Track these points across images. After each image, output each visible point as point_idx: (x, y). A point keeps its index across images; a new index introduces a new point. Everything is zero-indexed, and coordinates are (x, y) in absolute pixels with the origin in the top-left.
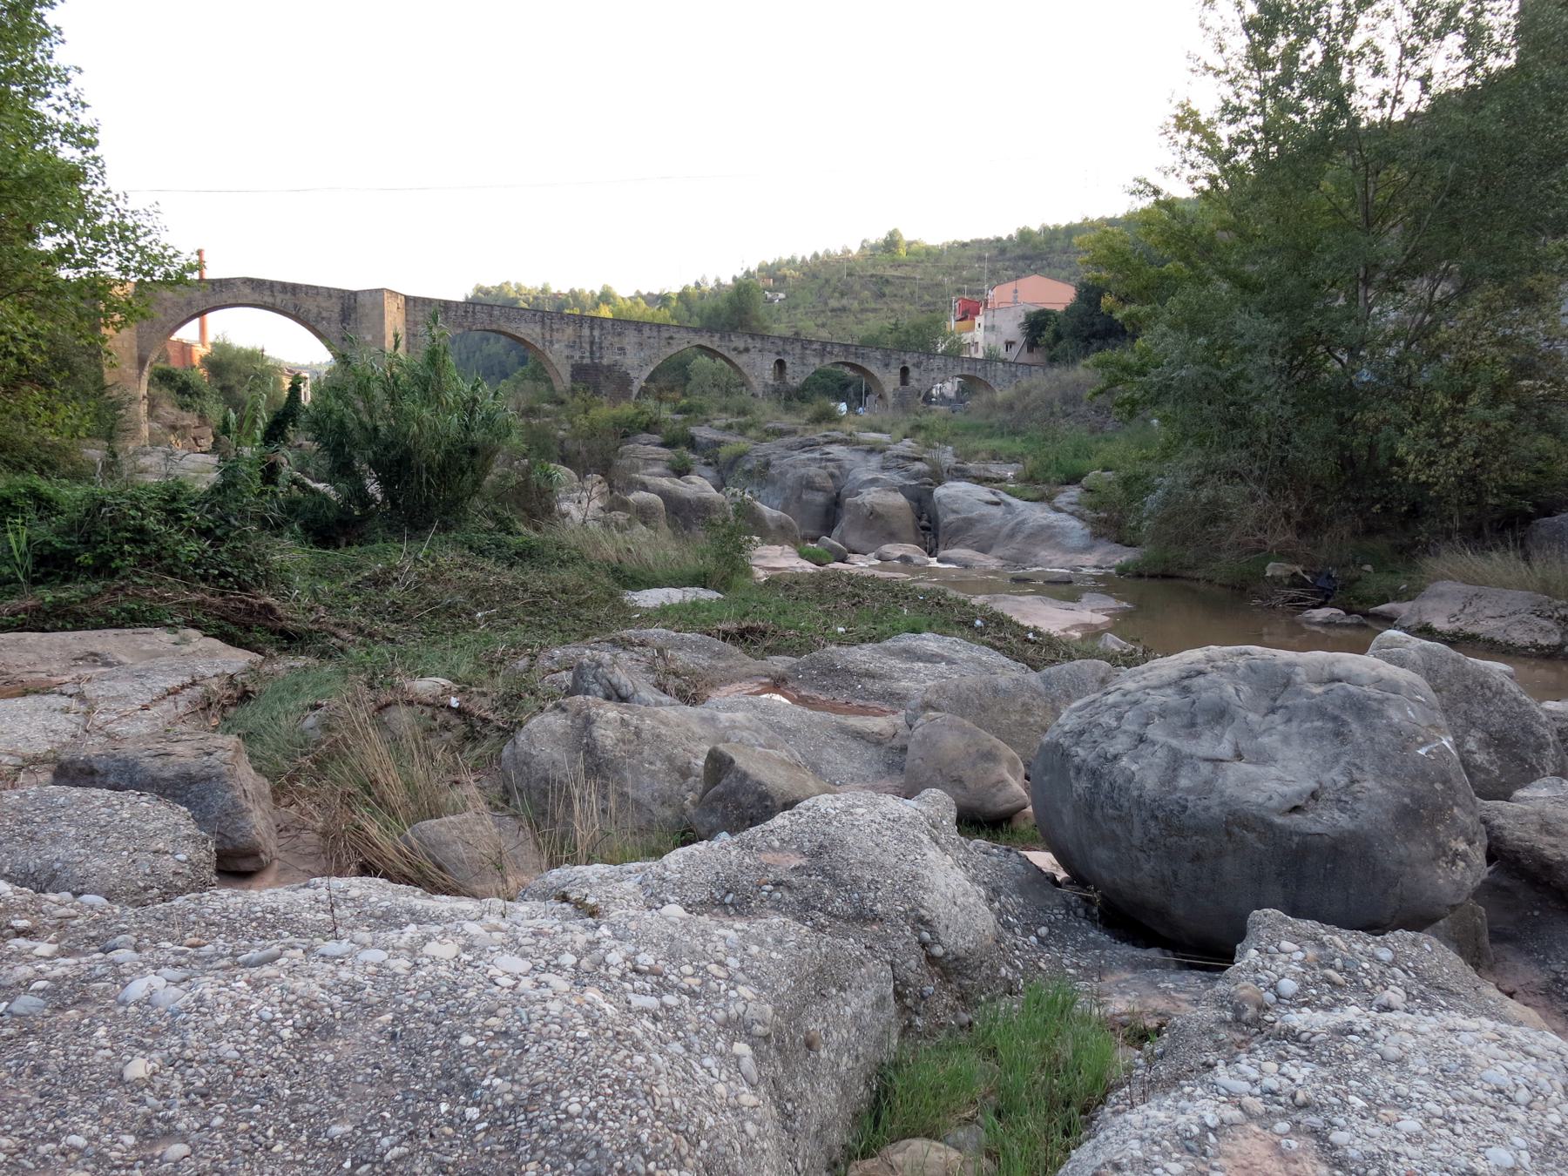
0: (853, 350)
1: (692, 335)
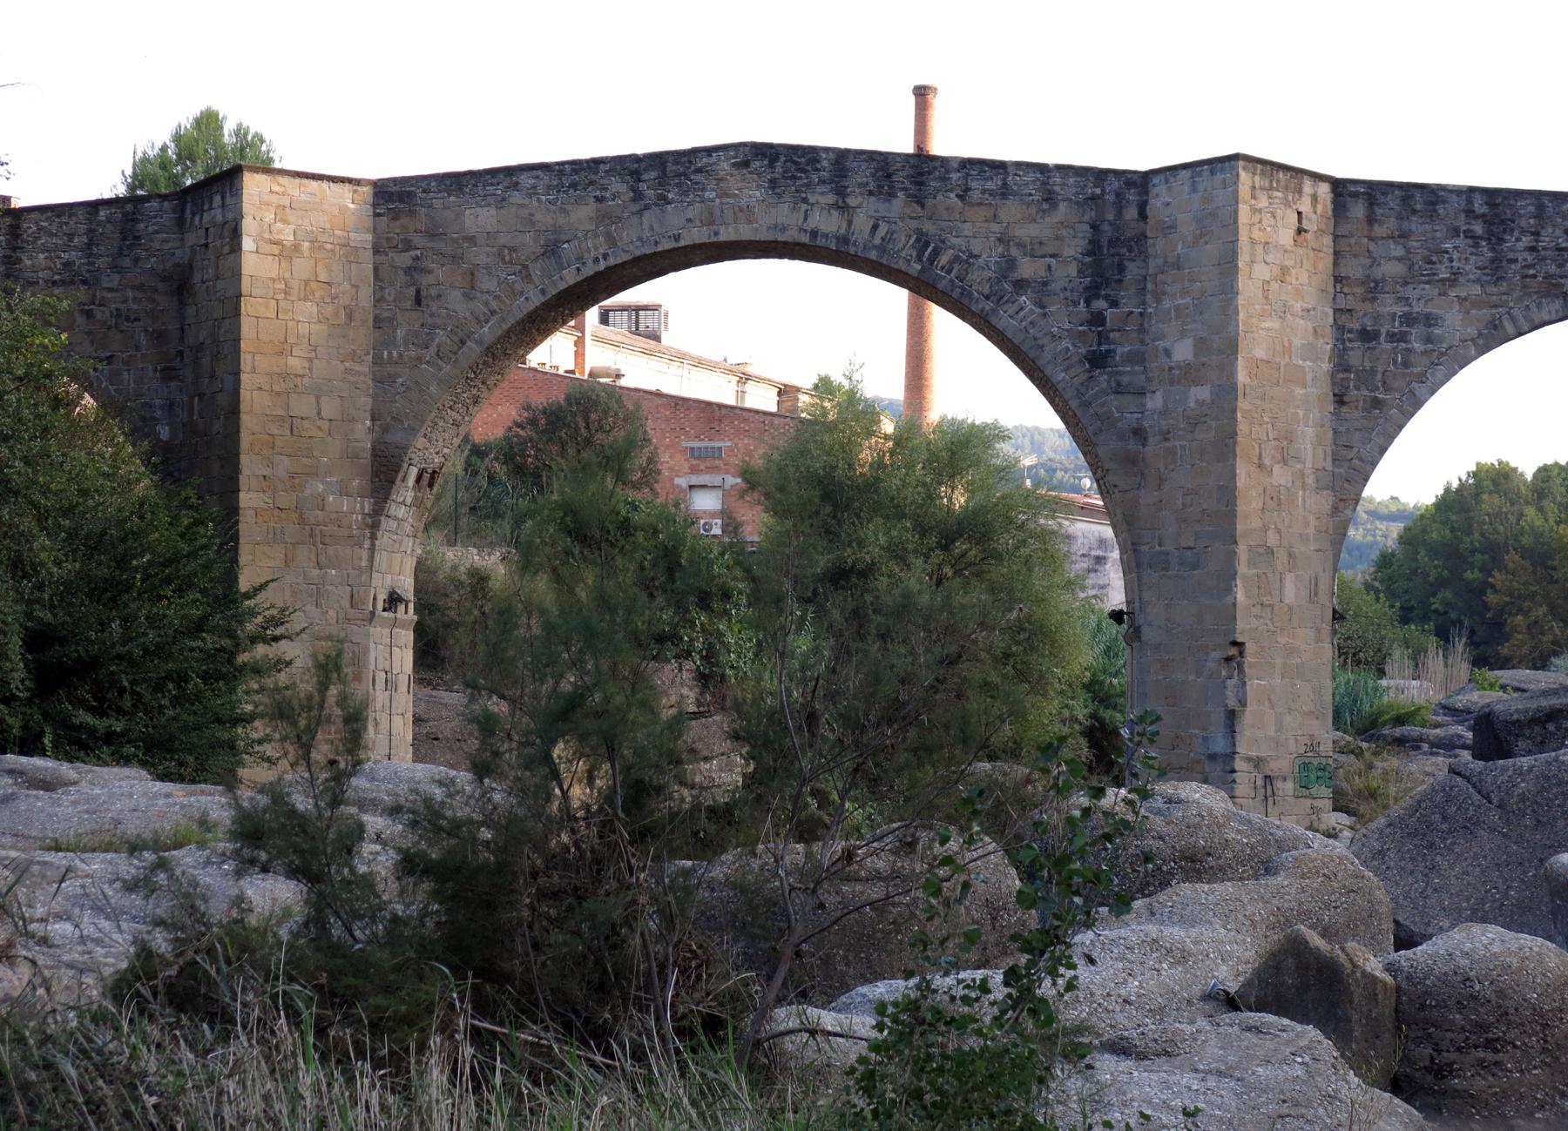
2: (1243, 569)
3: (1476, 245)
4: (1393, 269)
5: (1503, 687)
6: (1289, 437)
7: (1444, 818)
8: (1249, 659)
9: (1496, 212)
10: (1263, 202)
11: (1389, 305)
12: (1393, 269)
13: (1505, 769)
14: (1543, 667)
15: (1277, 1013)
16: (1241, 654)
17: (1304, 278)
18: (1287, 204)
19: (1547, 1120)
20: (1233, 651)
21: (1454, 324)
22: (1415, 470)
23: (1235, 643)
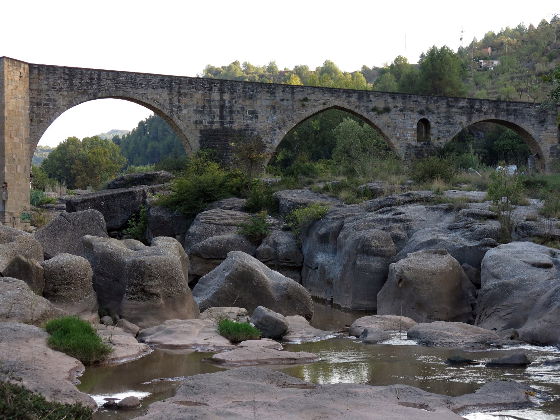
0: (504, 106)
1: (327, 96)
2: (6, 164)
3: (66, 81)
4: (44, 87)
5: (74, 194)
6: (18, 130)
7: (59, 227)
8: (8, 187)
9: (71, 73)
10: (11, 69)
11: (44, 96)
12: (44, 87)
13: (74, 215)
14: (85, 189)
15: (13, 277)
16: (6, 186)
17: (22, 89)
18: (17, 70)
19: (82, 302)
20: (4, 185)
21: (60, 101)
22: (53, 138)
23: (5, 183)
